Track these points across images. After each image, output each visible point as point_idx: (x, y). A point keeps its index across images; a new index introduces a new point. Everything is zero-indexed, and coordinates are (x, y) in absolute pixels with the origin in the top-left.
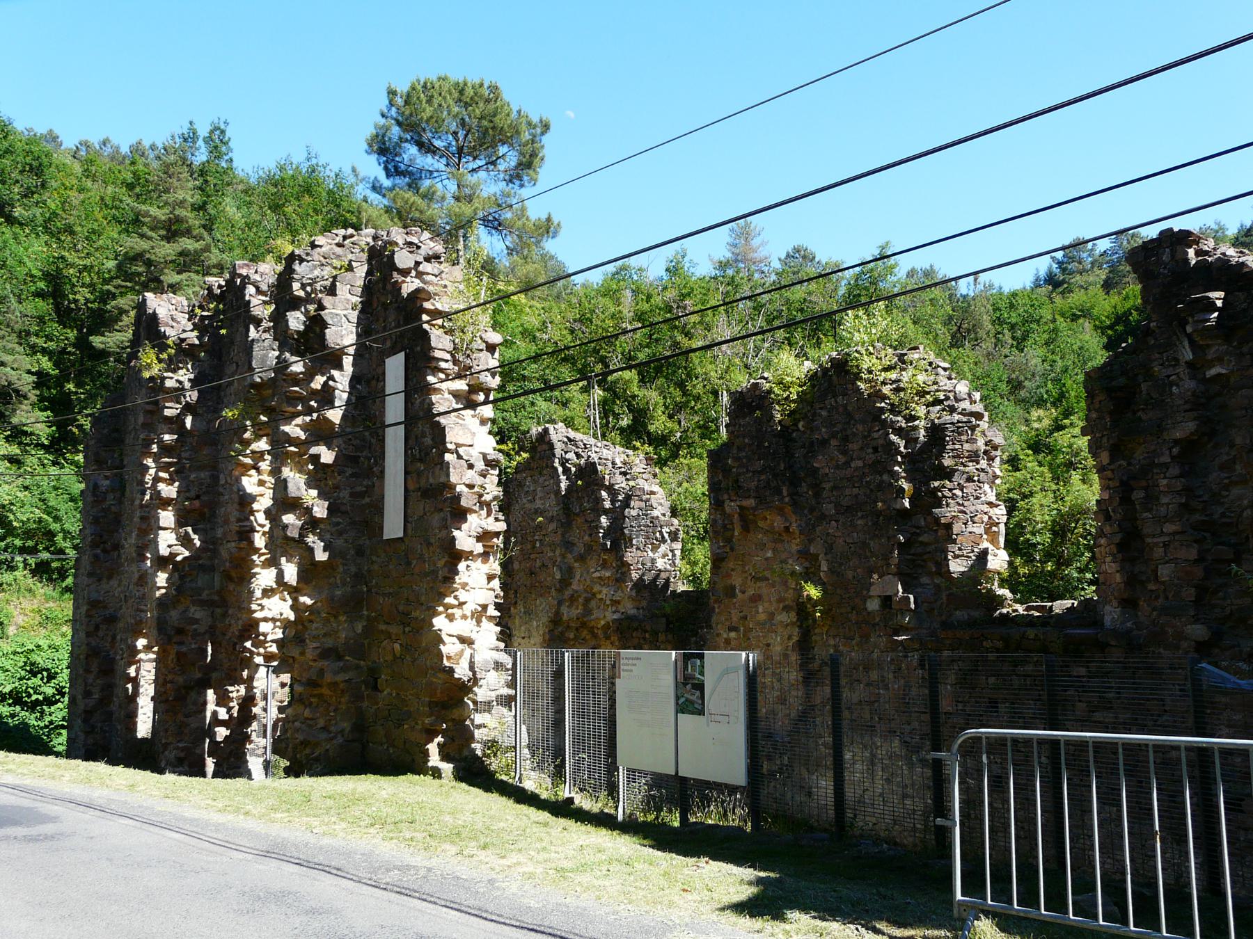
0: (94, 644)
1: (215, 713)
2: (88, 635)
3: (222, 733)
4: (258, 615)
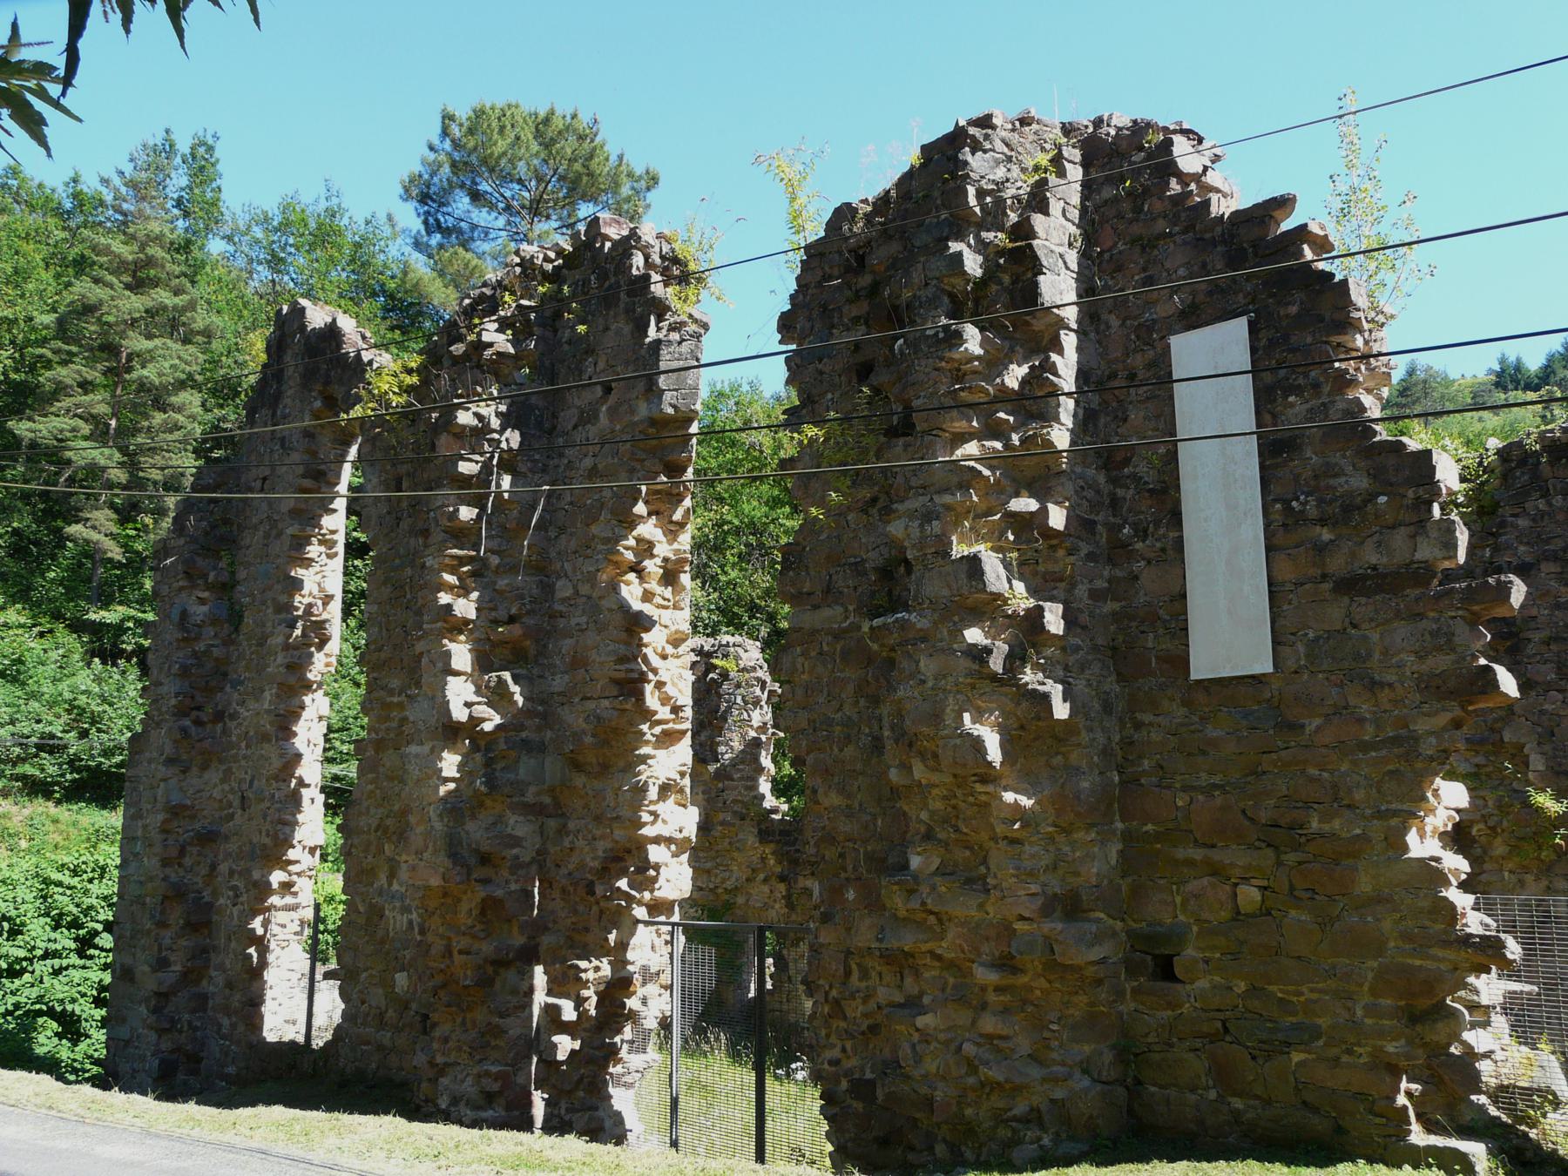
0: (174, 878)
1: (552, 1012)
2: (166, 862)
3: (565, 1045)
4: (648, 831)
